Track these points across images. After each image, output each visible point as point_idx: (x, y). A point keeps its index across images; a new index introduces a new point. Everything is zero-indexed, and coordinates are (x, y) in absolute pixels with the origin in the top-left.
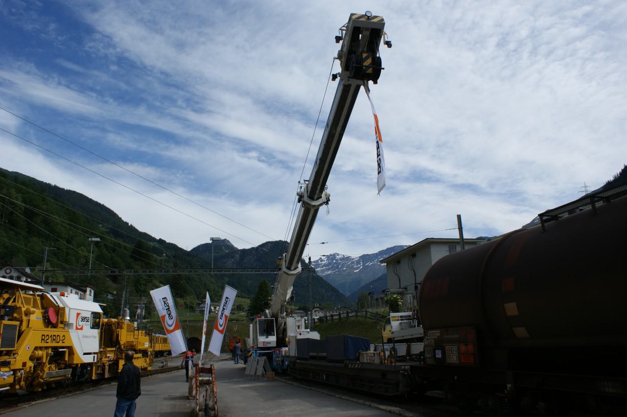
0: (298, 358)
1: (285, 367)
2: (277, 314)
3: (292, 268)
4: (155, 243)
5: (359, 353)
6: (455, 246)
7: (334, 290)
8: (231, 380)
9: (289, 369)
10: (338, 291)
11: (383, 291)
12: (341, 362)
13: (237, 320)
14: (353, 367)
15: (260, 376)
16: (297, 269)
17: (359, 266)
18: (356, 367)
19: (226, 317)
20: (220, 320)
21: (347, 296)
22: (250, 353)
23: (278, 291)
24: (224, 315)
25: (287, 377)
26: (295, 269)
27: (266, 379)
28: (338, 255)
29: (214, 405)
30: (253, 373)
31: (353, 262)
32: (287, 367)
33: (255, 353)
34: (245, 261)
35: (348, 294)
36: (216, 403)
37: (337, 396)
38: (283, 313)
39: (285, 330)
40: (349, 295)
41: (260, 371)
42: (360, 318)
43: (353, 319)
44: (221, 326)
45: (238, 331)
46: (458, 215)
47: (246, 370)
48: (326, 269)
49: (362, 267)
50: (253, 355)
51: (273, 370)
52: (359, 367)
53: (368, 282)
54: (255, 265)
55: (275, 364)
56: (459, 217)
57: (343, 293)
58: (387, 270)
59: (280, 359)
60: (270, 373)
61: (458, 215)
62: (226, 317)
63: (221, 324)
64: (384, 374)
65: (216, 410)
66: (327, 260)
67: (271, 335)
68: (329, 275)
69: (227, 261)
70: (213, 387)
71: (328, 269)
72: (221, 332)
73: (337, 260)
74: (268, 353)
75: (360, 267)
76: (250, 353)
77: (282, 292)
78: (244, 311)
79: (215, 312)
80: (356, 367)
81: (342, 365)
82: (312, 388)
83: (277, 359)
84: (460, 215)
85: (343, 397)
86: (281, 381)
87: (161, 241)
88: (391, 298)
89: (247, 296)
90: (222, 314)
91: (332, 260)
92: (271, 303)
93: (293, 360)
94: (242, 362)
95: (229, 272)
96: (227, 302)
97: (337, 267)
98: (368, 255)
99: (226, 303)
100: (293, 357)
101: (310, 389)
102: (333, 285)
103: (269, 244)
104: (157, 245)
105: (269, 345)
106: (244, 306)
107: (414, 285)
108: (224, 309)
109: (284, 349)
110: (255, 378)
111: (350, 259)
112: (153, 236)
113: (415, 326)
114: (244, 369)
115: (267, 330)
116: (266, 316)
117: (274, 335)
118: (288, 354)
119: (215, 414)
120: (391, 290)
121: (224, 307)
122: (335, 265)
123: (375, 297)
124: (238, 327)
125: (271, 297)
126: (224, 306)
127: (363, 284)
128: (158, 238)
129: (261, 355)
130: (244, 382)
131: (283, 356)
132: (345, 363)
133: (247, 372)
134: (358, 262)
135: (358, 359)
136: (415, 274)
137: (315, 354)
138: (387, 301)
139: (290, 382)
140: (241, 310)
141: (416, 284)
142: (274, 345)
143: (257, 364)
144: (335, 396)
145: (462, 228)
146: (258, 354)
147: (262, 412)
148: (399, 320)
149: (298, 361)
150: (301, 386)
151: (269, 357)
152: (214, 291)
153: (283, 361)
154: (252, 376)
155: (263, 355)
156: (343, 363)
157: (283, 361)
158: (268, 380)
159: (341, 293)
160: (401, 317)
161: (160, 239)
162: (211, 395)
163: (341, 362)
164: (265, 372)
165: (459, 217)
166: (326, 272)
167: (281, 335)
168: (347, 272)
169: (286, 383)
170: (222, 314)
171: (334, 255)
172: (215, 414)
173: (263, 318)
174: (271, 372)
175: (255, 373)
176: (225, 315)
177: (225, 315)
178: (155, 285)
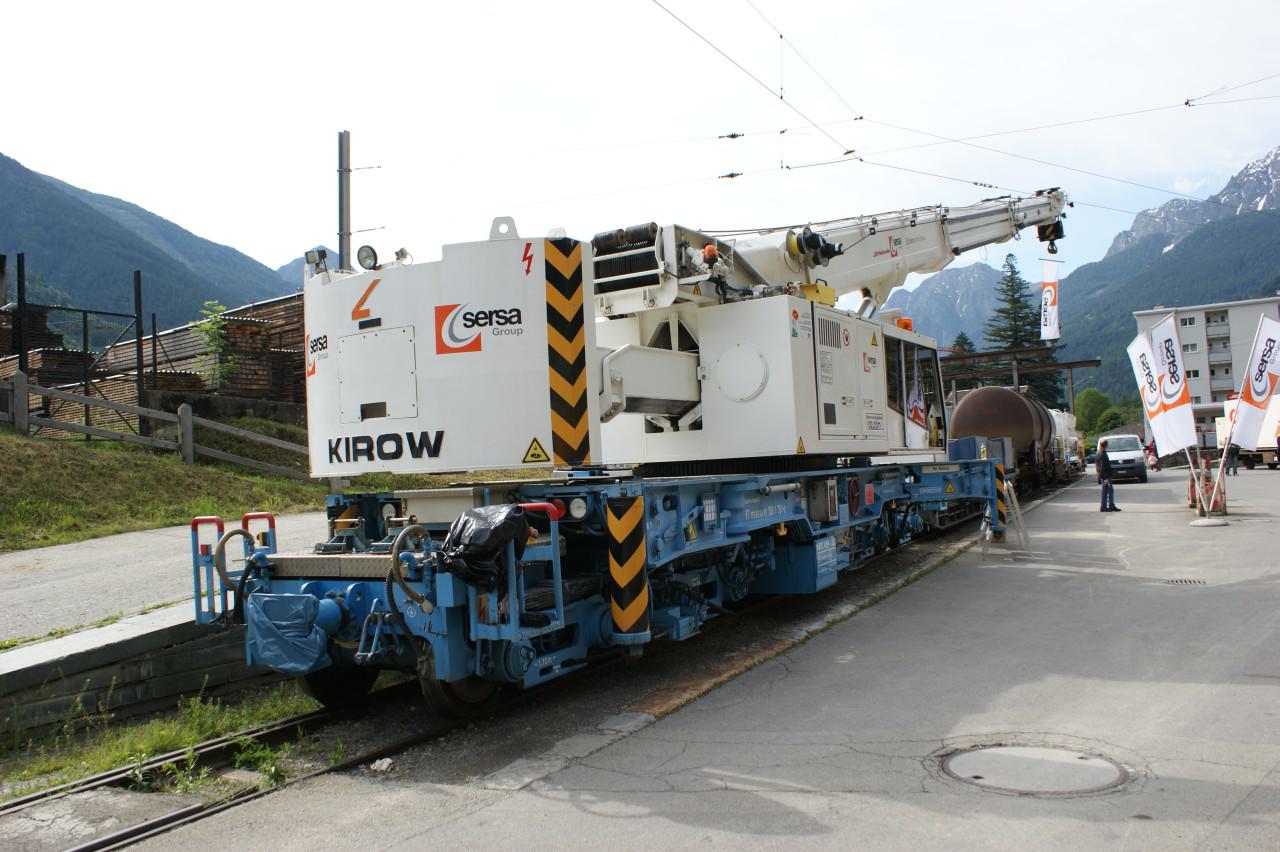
20: (1256, 384)
44: (1259, 394)
56: (344, 139)
63: (1259, 390)
90: (1261, 372)
96: (1271, 348)
121: (1265, 358)
126: (1264, 355)
165: (344, 139)
170: (1261, 372)
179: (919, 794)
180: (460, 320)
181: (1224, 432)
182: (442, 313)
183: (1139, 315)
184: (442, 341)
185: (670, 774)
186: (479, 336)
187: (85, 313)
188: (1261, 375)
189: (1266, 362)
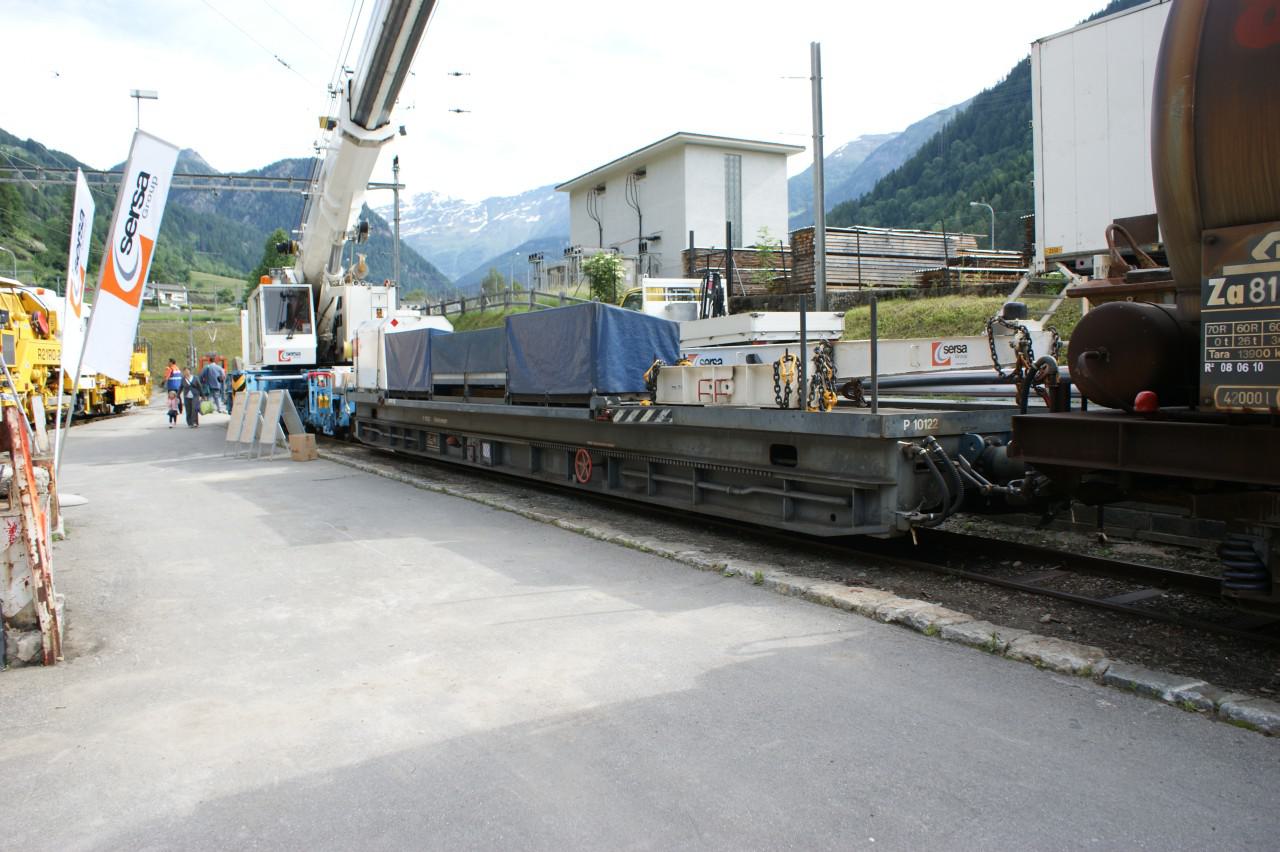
0: (391, 394)
1: (344, 420)
2: (321, 274)
3: (372, 123)
4: (18, 148)
5: (656, 370)
6: (740, 156)
7: (427, 267)
8: (186, 458)
9: (357, 424)
10: (434, 270)
11: (568, 251)
12: (581, 401)
13: (217, 320)
14: (630, 419)
15: (269, 445)
16: (385, 127)
17: (480, 220)
18: (645, 419)
19: (145, 242)
20: (122, 257)
21: (452, 281)
22: (241, 382)
23: (321, 203)
24: (136, 239)
25: (350, 449)
26: (379, 126)
27: (288, 454)
28: (437, 195)
29: (31, 604)
30: (249, 438)
31: (469, 212)
32: (351, 420)
33: (254, 382)
34: (235, 199)
35: (454, 277)
36: (42, 594)
37: (564, 523)
38: (337, 271)
39: (339, 321)
40: (457, 278)
41: (271, 432)
42: (517, 309)
43: (498, 312)
44: (128, 277)
45: (218, 343)
46: (813, 44)
47: (230, 427)
48: (412, 224)
49: (486, 223)
50: (248, 386)
51: (309, 428)
52: (659, 420)
53: (497, 254)
54: (257, 208)
55: (313, 411)
56: (816, 50)
57: (445, 274)
58: (571, 206)
59: (330, 397)
60: (301, 437)
61: (813, 44)
62: (145, 242)
63: (128, 270)
64: (784, 451)
65: (45, 626)
66: (414, 205)
67: (300, 330)
68: (417, 236)
69: (195, 198)
70: (23, 518)
71: (417, 224)
72: (130, 298)
73: (434, 206)
74: (292, 381)
75: (482, 222)
76: (241, 382)
77: (334, 205)
78: (233, 305)
79: (168, 305)
80: (630, 419)
81: (582, 414)
82: (450, 489)
83: (320, 399)
84: (818, 45)
85: (596, 530)
86: (334, 460)
87: (31, 146)
88: (598, 260)
89: (241, 275)
90: (130, 234)
91: (425, 204)
92: (301, 247)
93: (373, 399)
94: (223, 408)
95: (188, 183)
96: (144, 189)
97: (435, 221)
98: (499, 199)
99: (142, 194)
100: (369, 391)
101: (444, 492)
102: (424, 257)
103: (290, 166)
104: (23, 153)
105: (295, 361)
106: (234, 294)
107: (637, 242)
108: (134, 215)
109: (338, 371)
110: (255, 451)
111: (463, 206)
112: (11, 133)
113: (708, 317)
114: (225, 426)
115: (294, 312)
116: (285, 280)
117: (310, 332)
118: (350, 385)
119: (40, 647)
120: (586, 250)
121: (136, 209)
122: (430, 216)
123: (545, 265)
124: (218, 333)
125: (299, 228)
126: (134, 204)
127: (487, 258)
128: (24, 138)
129: (271, 386)
130: (221, 466)
131: (337, 391)
132: (593, 406)
133: (232, 436)
134: (479, 213)
135: (651, 388)
136: (640, 217)
137: (456, 378)
138: (587, 268)
139: (366, 466)
140: (226, 301)
141: (641, 239)
142: (310, 358)
143: (259, 410)
144: (553, 523)
145: (820, 79)
146: (263, 384)
147: (280, 614)
148: (664, 299)
149: (392, 401)
150: (405, 477)
151: (299, 393)
152: (166, 260)
153: (337, 404)
154: (245, 445)
155: (281, 385)
156: (587, 406)
157: (337, 404)
158: (296, 458)
159: (441, 275)
160: (671, 289)
161: (30, 141)
162: (14, 558)
163: (581, 401)
164: (286, 432)
165: (816, 50)
166: (412, 229)
167: (329, 335)
168: (454, 231)
169: (354, 466)
170: (130, 234)
171: (430, 194)
172: (40, 647)
173: (277, 283)
174: (305, 435)
175: (257, 437)
176: (142, 238)
177: (142, 238)
178: (22, 242)
179: (536, 242)
180: (942, 350)
181: (866, 310)
182: (280, 352)
183: (627, 476)
184: (23, 142)
185: (345, 477)
186: (141, 236)
187: (700, 394)
188: (130, 241)
189: (137, 216)
